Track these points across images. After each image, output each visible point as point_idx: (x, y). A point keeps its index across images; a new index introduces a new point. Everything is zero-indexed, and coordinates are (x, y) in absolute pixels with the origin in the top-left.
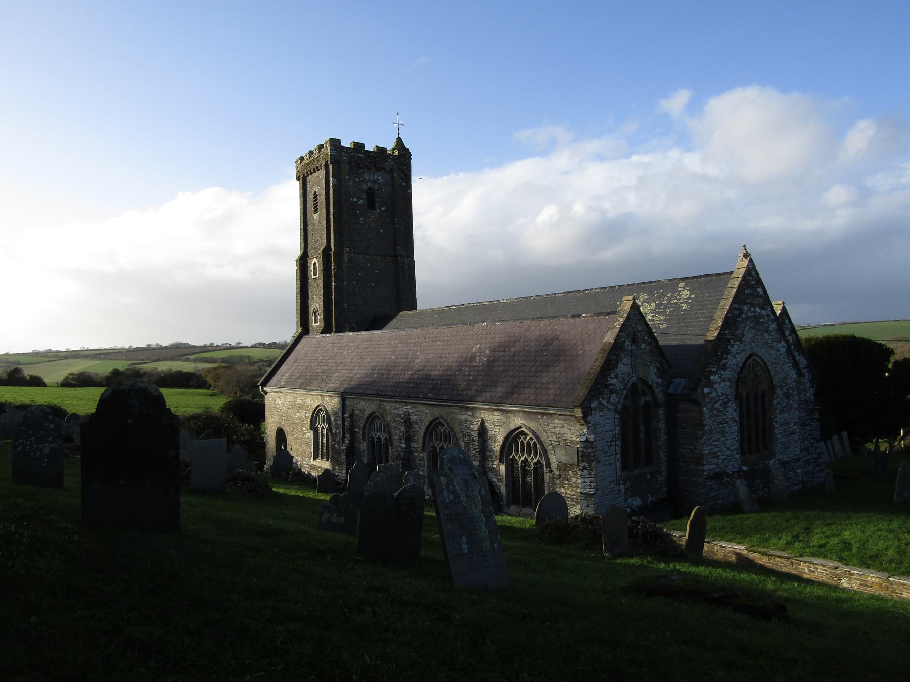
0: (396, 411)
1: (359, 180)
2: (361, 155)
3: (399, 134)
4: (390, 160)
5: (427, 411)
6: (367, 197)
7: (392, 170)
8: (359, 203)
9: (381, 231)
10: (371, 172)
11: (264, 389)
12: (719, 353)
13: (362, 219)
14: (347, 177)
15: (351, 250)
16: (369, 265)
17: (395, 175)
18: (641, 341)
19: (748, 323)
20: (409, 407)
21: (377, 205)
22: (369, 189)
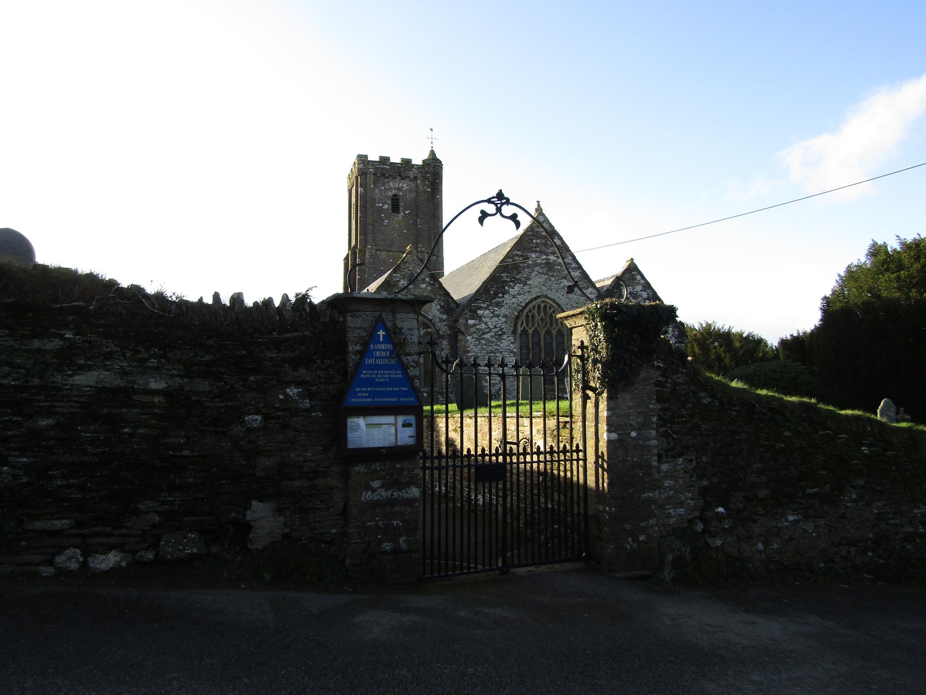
1: (385, 188)
2: (387, 167)
3: (432, 147)
4: (414, 170)
6: (392, 202)
7: (415, 178)
8: (384, 207)
9: (405, 231)
10: (397, 180)
12: (492, 292)
13: (386, 221)
14: (372, 186)
15: (372, 247)
16: (391, 260)
17: (418, 182)
18: (421, 281)
19: (537, 269)
21: (401, 208)
22: (395, 195)
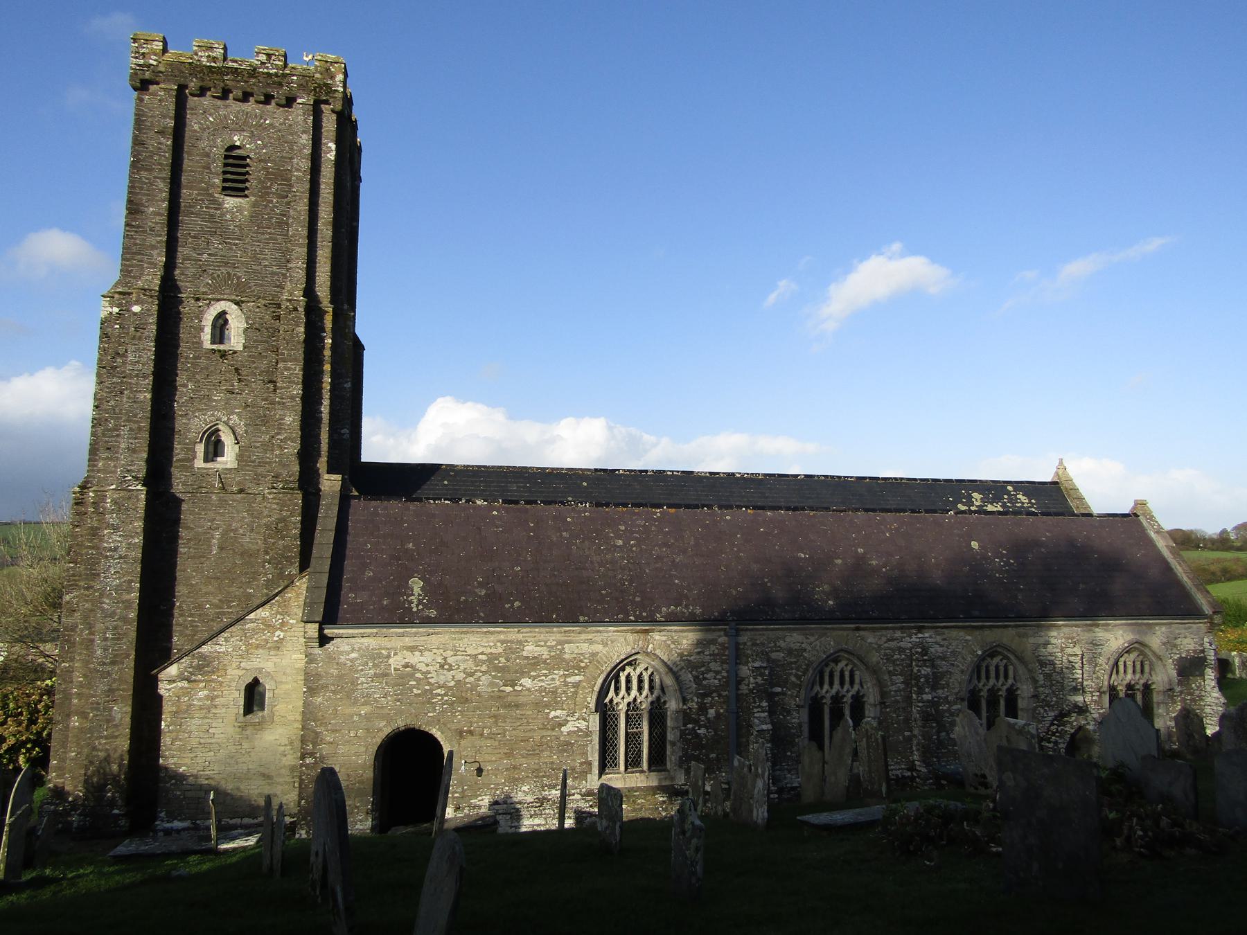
0: (892, 644)
5: (969, 638)
11: (326, 631)
20: (927, 635)
